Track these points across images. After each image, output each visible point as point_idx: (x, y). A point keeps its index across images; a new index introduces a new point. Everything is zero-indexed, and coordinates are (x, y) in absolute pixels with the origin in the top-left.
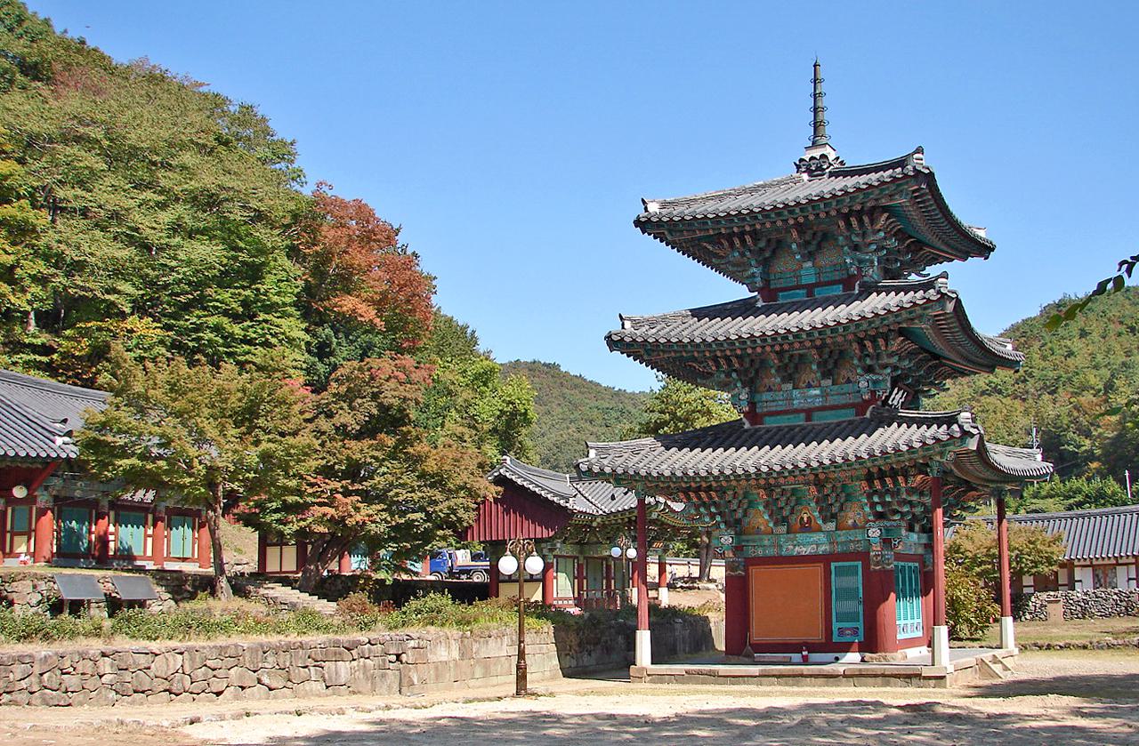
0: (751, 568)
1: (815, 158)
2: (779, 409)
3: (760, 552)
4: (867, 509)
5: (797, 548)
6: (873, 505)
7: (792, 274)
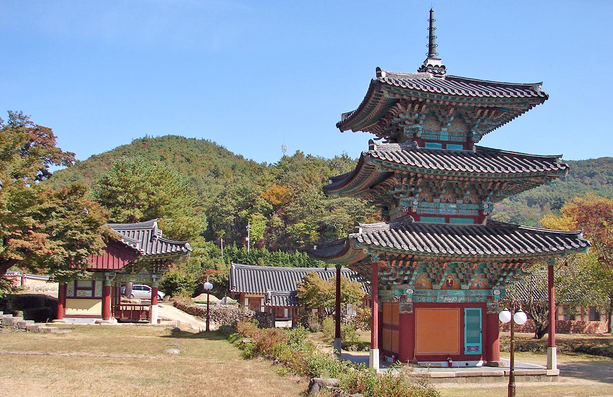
0: (416, 309)
1: (432, 66)
2: (430, 213)
3: (423, 300)
4: (413, 278)
5: (446, 298)
6: (411, 276)
7: (435, 133)
